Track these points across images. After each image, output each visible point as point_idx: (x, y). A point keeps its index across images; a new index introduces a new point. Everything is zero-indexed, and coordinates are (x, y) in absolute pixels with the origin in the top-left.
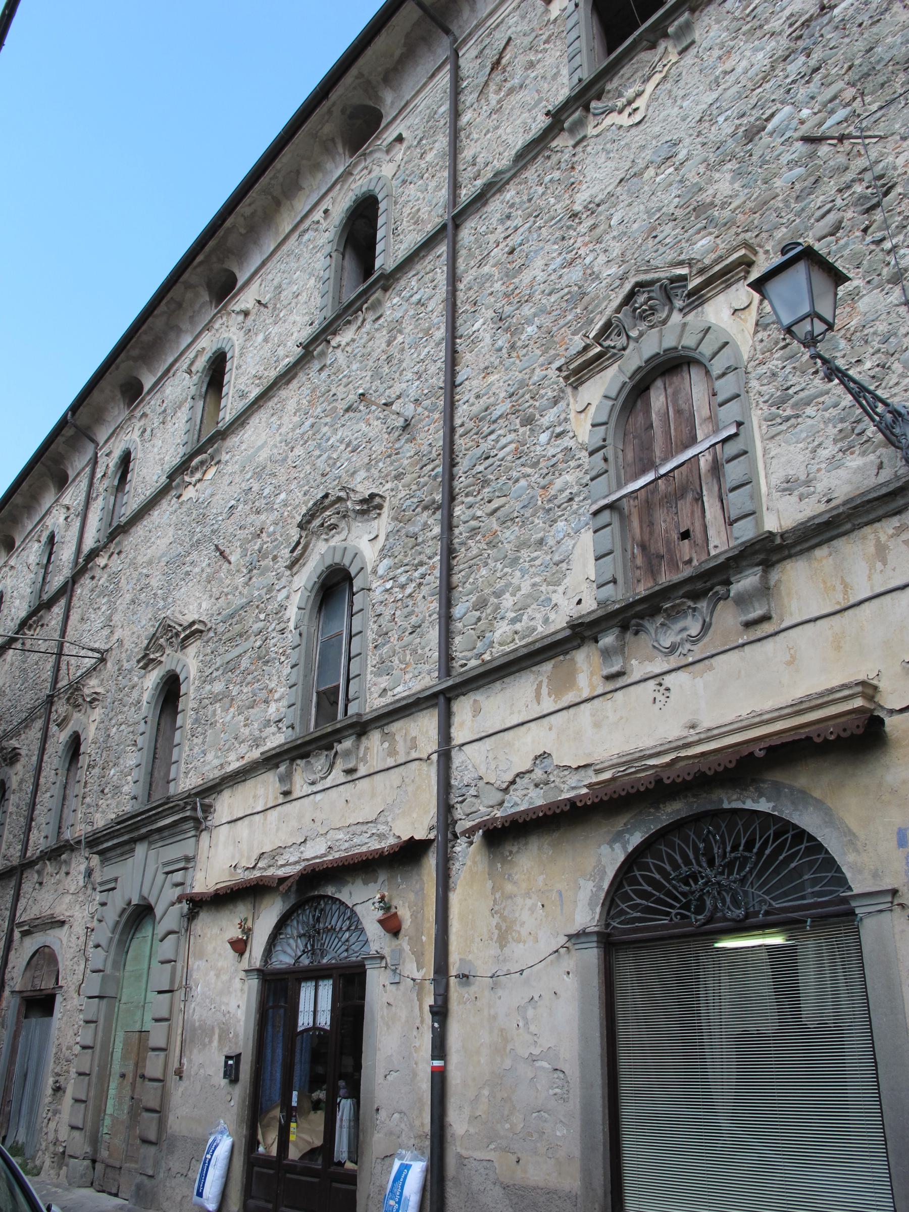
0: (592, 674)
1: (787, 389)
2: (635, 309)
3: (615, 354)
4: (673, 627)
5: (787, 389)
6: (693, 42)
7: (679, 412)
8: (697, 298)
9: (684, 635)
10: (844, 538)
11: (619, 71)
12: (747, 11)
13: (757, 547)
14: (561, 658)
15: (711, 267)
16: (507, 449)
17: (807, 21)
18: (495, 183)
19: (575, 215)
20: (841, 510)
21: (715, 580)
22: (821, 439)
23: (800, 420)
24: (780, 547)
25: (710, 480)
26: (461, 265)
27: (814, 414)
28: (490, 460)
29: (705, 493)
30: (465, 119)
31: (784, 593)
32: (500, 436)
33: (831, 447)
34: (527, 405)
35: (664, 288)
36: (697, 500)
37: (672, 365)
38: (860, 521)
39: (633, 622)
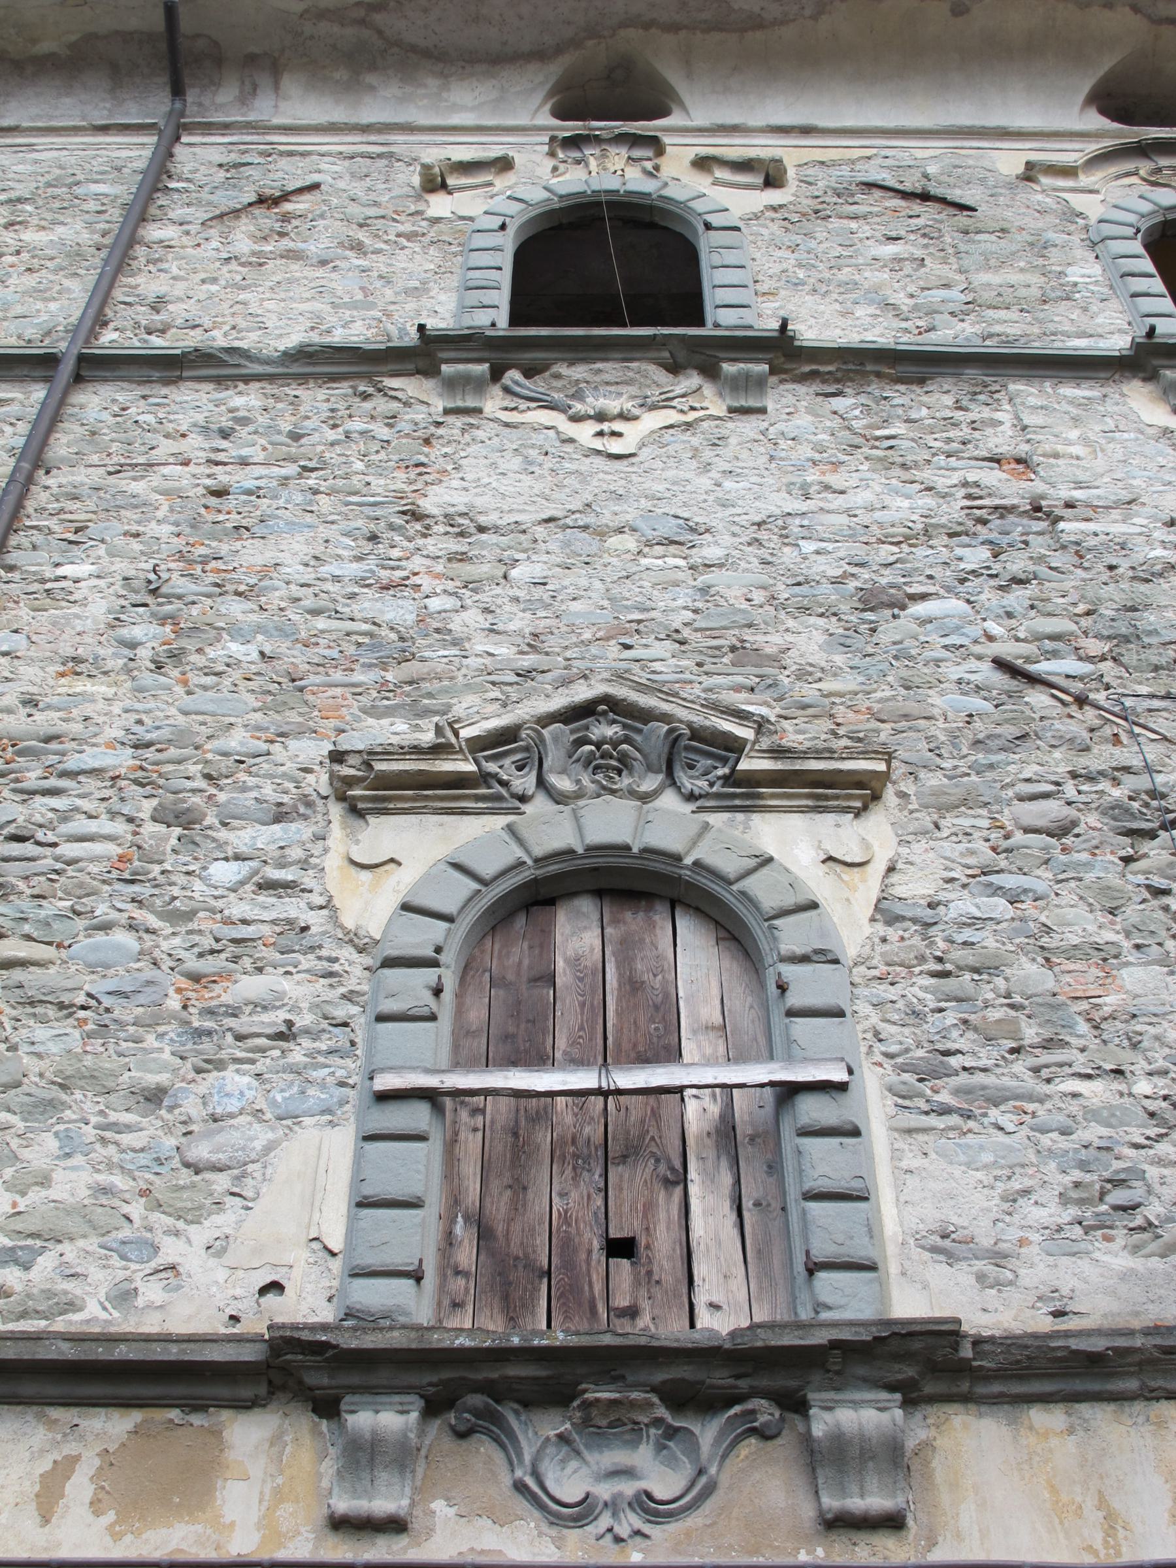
0: (279, 1496)
1: (947, 1053)
2: (580, 742)
3: (499, 798)
4: (591, 1457)
5: (947, 1053)
6: (763, 411)
7: (633, 986)
8: (745, 793)
9: (629, 1488)
10: (1111, 1407)
11: (594, 360)
12: (878, 433)
13: (917, 1345)
14: (174, 1414)
15: (804, 755)
16: (97, 848)
17: (1004, 508)
18: (222, 363)
19: (416, 515)
20: (1138, 1342)
21: (764, 1382)
22: (1028, 1183)
23: (971, 1124)
24: (962, 1369)
25: (711, 1154)
26: (61, 445)
27: (1010, 1127)
28: (28, 849)
29: (693, 1174)
30: (154, 232)
31: (939, 1476)
32: (76, 809)
33: (1054, 1207)
34: (189, 784)
35: (674, 740)
36: (668, 1183)
37: (634, 884)
38: (1160, 1383)
39: (477, 1400)
